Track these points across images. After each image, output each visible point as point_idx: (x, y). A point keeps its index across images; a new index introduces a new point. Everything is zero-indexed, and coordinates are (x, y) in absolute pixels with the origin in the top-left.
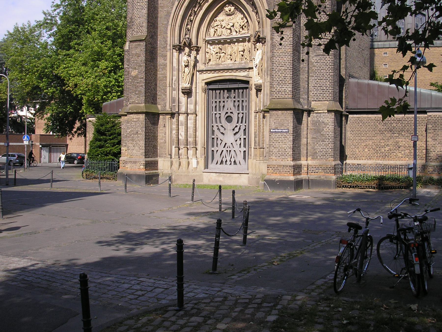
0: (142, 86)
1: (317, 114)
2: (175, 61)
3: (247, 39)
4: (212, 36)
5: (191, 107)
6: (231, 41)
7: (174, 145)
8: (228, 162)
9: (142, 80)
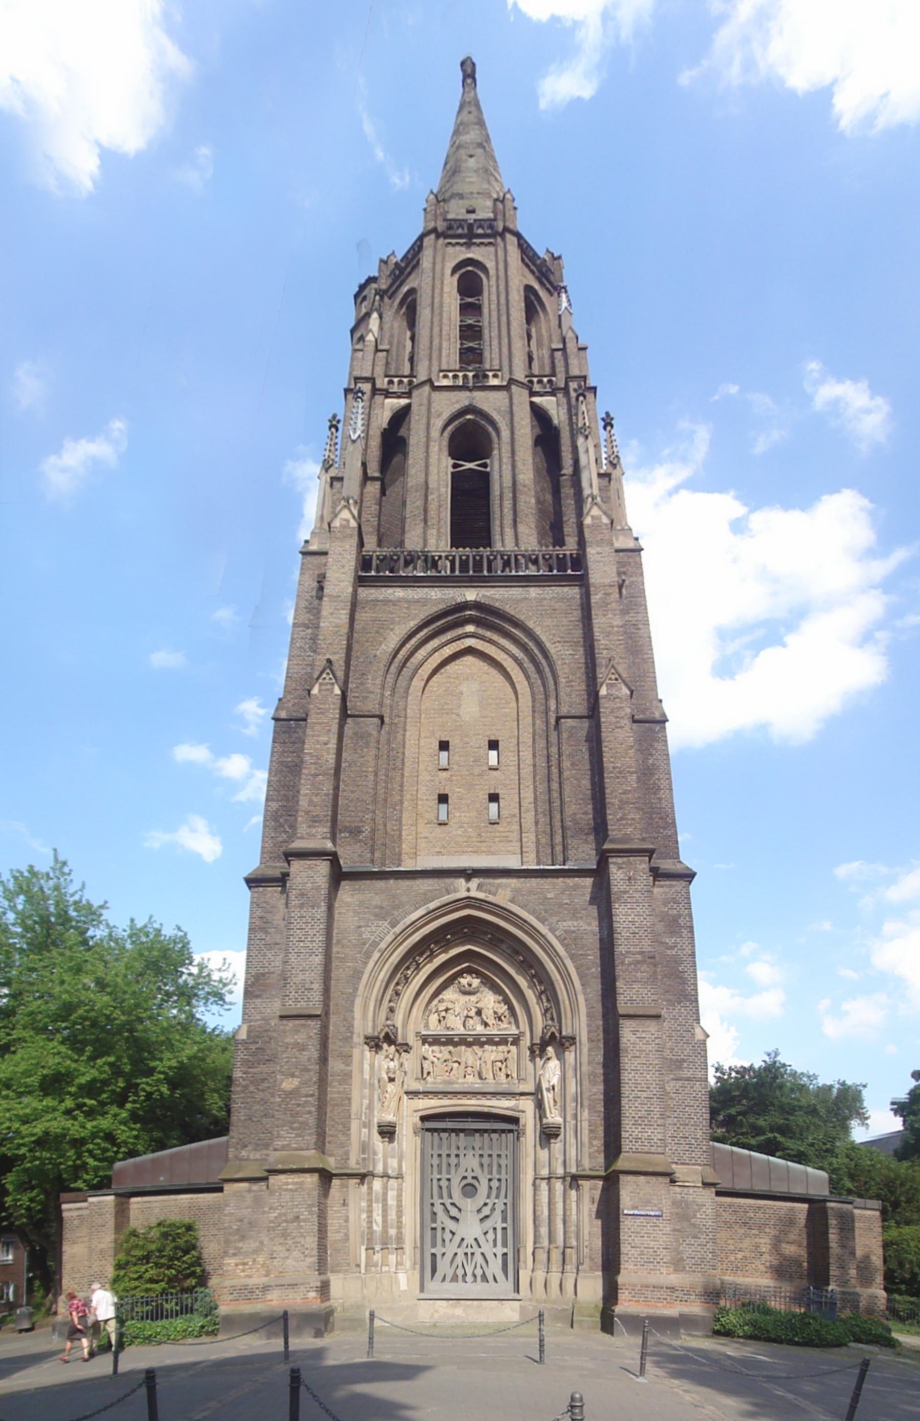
0: (309, 1112)
1: (682, 1189)
2: (366, 1067)
3: (510, 1039)
4: (434, 1028)
5: (393, 1163)
6: (478, 1042)
7: (363, 1244)
8: (469, 1278)
9: (310, 1099)
